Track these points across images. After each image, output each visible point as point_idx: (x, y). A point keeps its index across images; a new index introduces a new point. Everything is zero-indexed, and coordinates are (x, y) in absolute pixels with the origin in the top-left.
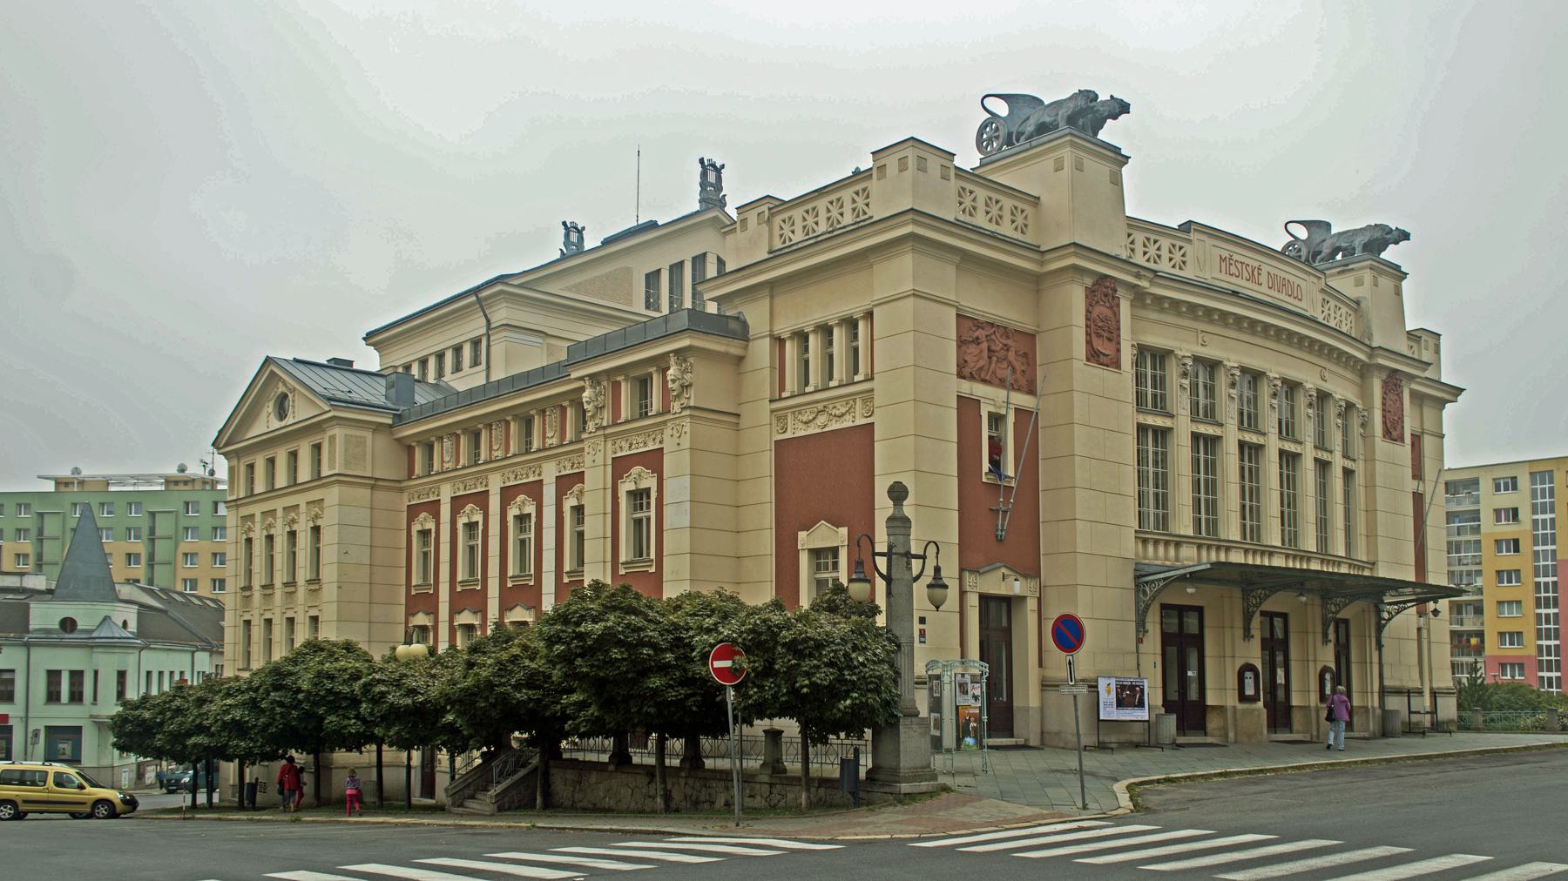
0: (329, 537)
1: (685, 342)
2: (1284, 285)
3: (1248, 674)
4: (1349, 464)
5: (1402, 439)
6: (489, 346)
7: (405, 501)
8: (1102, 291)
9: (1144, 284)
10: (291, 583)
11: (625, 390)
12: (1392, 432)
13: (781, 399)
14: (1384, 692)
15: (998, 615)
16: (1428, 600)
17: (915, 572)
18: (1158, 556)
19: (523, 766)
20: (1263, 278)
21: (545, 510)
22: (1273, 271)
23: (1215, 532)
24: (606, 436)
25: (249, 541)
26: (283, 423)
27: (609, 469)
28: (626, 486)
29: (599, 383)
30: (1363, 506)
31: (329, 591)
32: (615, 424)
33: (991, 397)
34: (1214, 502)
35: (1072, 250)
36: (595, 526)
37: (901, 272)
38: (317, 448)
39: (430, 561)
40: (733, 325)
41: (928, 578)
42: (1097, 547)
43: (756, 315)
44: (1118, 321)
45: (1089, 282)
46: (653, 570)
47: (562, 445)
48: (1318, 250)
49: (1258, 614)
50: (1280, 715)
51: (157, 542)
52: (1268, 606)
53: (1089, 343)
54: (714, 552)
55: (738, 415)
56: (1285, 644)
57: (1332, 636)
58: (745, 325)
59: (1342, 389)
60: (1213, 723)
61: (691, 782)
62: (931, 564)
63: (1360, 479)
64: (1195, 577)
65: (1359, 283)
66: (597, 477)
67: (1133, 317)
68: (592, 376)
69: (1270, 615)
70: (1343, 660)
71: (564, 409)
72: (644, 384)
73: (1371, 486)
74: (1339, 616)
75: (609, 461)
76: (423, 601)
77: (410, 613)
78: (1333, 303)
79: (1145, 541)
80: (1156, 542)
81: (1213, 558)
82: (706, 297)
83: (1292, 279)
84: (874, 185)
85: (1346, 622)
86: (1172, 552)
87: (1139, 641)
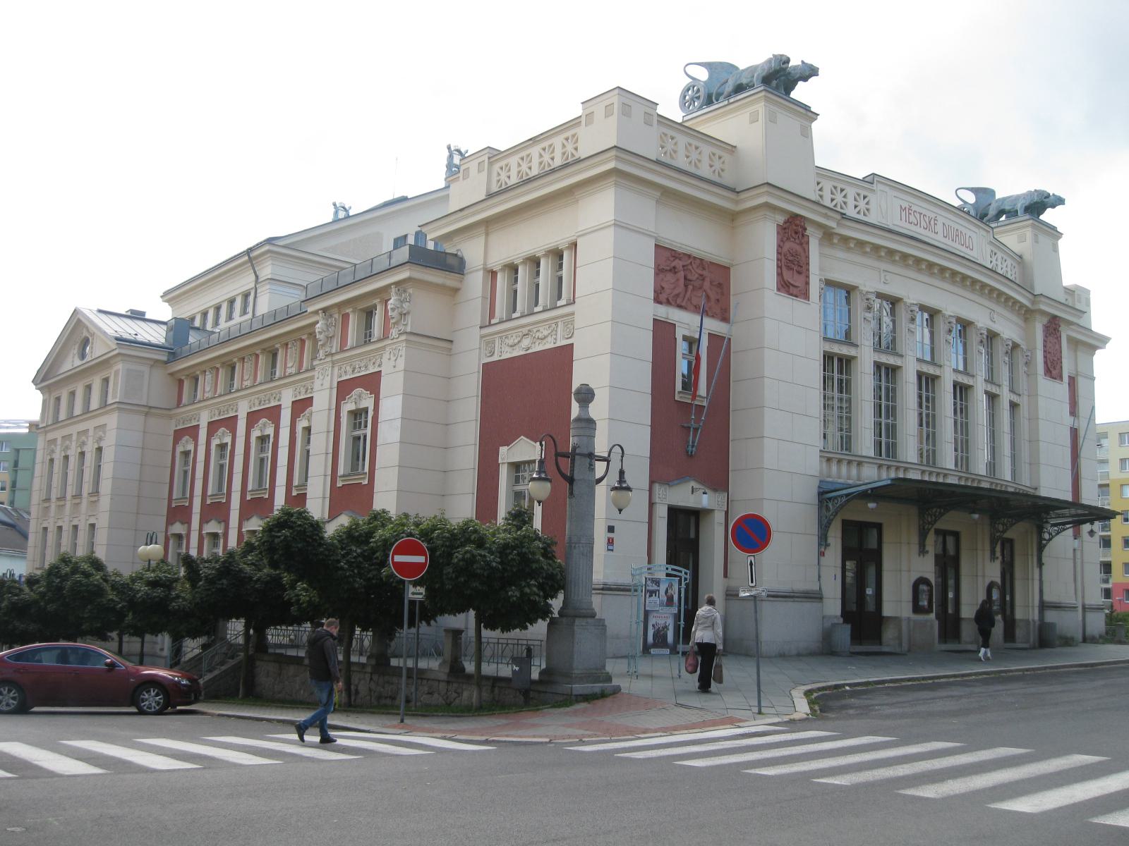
0: (108, 455)
1: (404, 274)
2: (958, 234)
3: (923, 587)
4: (1015, 399)
5: (1061, 378)
6: (255, 297)
7: (173, 426)
8: (793, 230)
9: (832, 224)
10: (78, 495)
11: (353, 322)
12: (1053, 369)
13: (490, 325)
14: (1044, 606)
15: (684, 533)
16: (1084, 522)
17: (598, 474)
18: (845, 475)
19: (232, 657)
20: (939, 228)
21: (281, 431)
22: (948, 223)
23: (894, 456)
24: (333, 363)
25: (52, 460)
26: (84, 362)
27: (335, 391)
28: (348, 406)
29: (331, 316)
30: (1027, 437)
31: (105, 502)
32: (342, 351)
33: (686, 322)
34: (894, 426)
35: (765, 189)
36: (320, 444)
37: (601, 208)
38: (106, 380)
39: (189, 478)
40: (450, 261)
41: (613, 479)
42: (785, 451)
43: (472, 251)
44: (808, 257)
45: (781, 219)
46: (366, 482)
47: (299, 373)
48: (987, 211)
49: (932, 532)
50: (950, 627)
51: (20, 473)
52: (940, 525)
53: (780, 274)
54: (420, 465)
55: (452, 341)
56: (956, 561)
57: (998, 554)
58: (462, 261)
59: (1008, 329)
60: (889, 634)
61: (375, 677)
62: (615, 466)
63: (1024, 411)
64: (876, 494)
65: (1022, 240)
66: (323, 399)
67: (821, 254)
68: (325, 310)
69: (943, 534)
70: (1008, 577)
71: (303, 341)
72: (369, 313)
73: (1034, 419)
74: (1008, 535)
75: (335, 385)
76: (179, 513)
77: (170, 522)
78: (1000, 255)
79: (829, 460)
80: (840, 461)
81: (893, 475)
82: (428, 238)
83: (964, 231)
84: (581, 131)
85: (1011, 541)
86: (854, 471)
87: (821, 554)
